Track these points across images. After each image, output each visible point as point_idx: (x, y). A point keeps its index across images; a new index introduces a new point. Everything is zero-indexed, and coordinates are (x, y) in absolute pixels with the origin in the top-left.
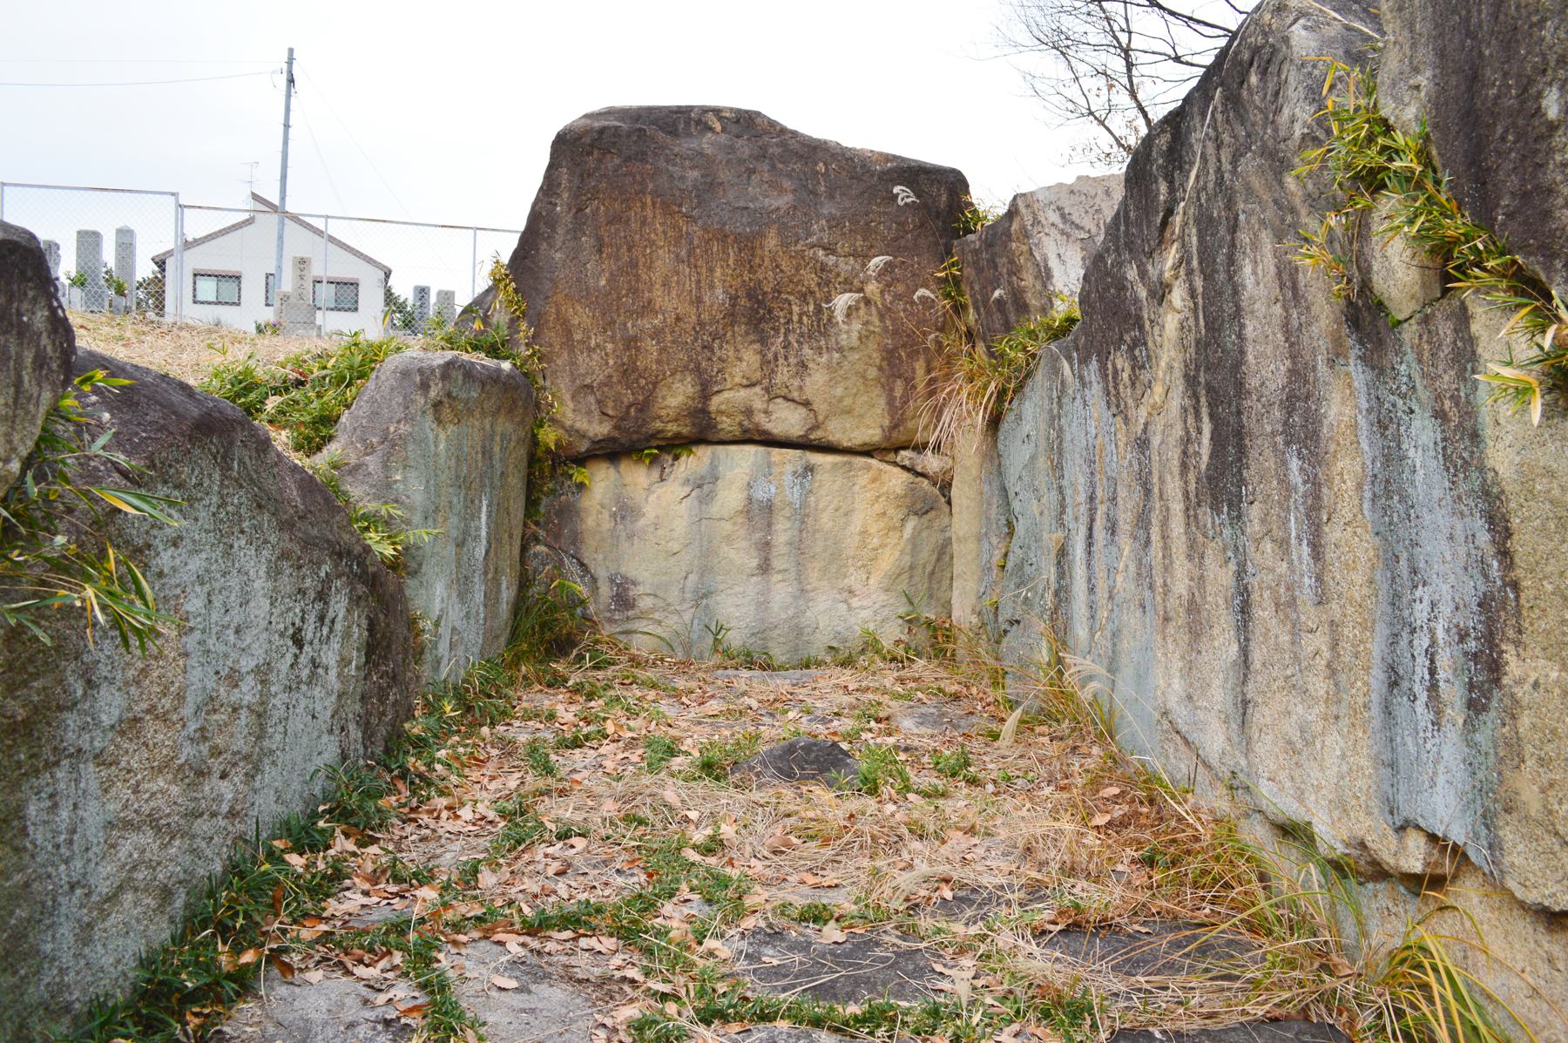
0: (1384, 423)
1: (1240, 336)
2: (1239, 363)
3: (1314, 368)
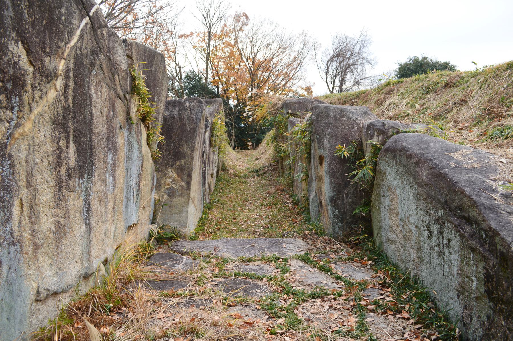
0: (130, 144)
1: (91, 113)
2: (91, 123)
3: (116, 129)
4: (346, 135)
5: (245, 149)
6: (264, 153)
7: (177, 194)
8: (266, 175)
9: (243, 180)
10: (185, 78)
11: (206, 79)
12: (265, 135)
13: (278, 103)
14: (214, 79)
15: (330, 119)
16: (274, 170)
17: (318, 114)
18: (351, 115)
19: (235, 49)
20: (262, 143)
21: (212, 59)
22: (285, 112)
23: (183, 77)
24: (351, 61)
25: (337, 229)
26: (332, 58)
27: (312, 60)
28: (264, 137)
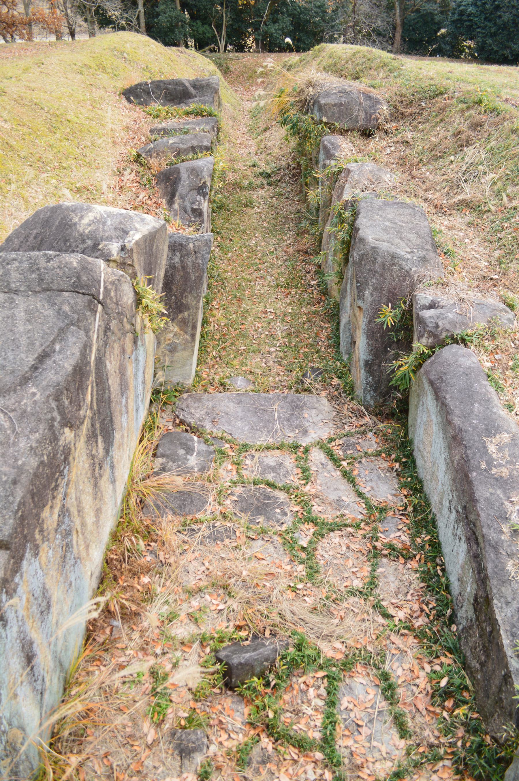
4: (395, 289)
7: (180, 348)
15: (377, 265)
16: (294, 175)
17: (363, 255)
18: (404, 263)
25: (368, 397)
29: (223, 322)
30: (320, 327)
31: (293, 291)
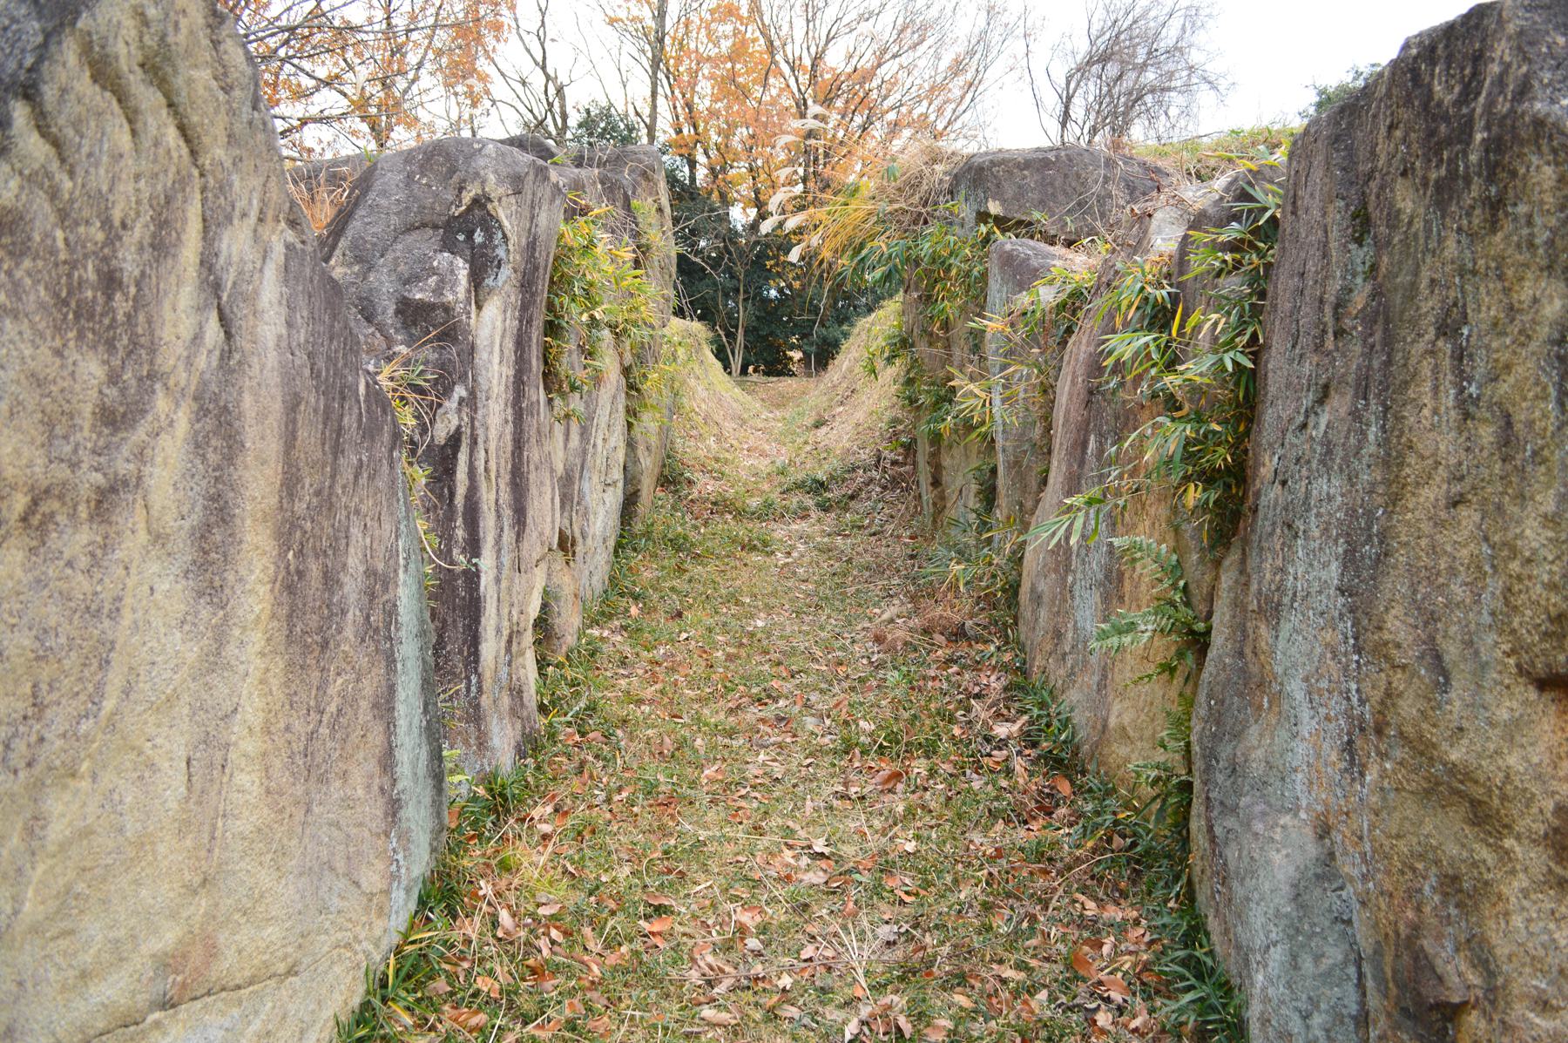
5: (779, 374)
6: (851, 401)
8: (860, 506)
9: (757, 527)
10: (580, 126)
11: (651, 130)
12: (852, 325)
13: (927, 171)
14: (679, 131)
16: (895, 482)
19: (752, 32)
20: (839, 357)
21: (672, 62)
22: (966, 211)
23: (573, 122)
24: (1150, 76)
26: (1082, 70)
27: (1015, 75)
28: (846, 335)
29: (554, 899)
30: (1082, 922)
31: (920, 767)
